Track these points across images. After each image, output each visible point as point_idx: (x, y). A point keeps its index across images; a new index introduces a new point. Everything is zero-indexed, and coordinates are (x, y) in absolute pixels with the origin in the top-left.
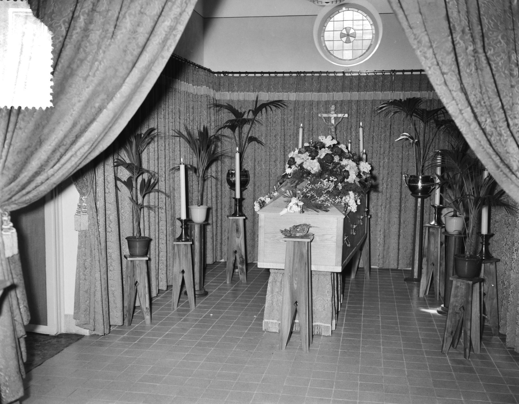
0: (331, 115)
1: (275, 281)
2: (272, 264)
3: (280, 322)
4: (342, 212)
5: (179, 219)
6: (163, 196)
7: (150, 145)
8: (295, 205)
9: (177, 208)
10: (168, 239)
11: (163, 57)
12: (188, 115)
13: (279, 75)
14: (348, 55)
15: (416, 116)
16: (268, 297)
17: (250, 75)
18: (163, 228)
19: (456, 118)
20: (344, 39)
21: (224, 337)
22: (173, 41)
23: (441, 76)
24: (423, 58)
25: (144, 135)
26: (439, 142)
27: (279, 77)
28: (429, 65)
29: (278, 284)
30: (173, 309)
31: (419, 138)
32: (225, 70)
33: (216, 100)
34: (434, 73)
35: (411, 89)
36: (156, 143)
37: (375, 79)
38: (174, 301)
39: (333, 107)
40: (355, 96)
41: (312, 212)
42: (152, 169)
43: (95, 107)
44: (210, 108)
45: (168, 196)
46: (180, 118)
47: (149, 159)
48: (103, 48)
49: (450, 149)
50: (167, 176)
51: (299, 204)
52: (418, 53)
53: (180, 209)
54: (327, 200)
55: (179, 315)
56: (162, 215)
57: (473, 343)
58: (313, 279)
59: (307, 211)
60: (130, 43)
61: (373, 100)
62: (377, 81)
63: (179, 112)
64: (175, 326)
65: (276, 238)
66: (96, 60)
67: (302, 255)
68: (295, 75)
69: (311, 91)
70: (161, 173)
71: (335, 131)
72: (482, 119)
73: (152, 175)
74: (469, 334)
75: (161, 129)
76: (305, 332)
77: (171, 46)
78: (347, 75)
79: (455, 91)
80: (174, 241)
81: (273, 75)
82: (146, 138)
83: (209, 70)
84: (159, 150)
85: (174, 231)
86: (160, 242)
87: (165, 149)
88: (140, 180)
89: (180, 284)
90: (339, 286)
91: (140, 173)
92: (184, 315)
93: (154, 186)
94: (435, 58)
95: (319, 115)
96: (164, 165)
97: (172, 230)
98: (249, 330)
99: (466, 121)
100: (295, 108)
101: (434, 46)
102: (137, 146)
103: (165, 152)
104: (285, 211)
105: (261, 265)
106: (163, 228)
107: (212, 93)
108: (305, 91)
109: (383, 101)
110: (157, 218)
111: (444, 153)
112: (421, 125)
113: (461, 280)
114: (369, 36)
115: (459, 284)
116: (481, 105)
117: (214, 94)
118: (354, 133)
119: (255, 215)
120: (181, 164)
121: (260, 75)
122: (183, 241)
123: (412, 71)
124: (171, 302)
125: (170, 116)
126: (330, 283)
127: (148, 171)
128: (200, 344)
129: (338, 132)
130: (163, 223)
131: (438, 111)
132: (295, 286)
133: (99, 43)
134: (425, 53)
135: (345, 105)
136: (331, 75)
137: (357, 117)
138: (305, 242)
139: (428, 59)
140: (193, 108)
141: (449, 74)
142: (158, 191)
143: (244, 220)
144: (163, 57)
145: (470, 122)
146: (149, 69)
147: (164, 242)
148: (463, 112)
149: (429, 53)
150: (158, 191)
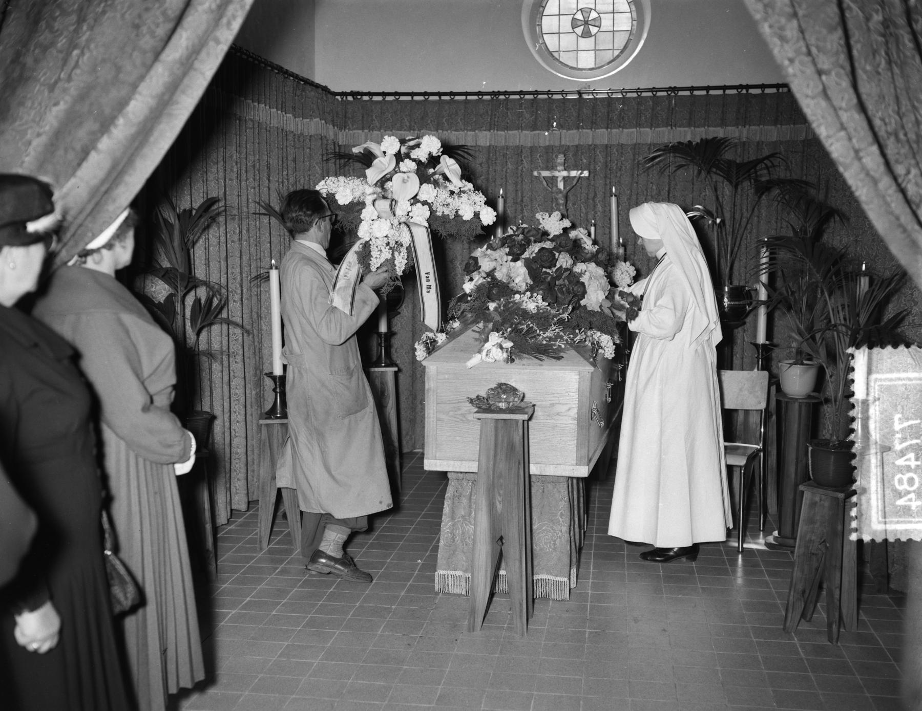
0: (556, 174)
1: (458, 496)
2: (452, 462)
3: (469, 575)
4: (587, 359)
5: (270, 375)
6: (238, 331)
7: (211, 231)
8: (496, 346)
9: (265, 352)
10: (249, 412)
11: (218, 42)
12: (285, 173)
13: (457, 98)
14: (586, 60)
15: (716, 173)
16: (446, 525)
17: (402, 98)
18: (238, 391)
19: (846, 167)
20: (579, 30)
21: (360, 606)
22: (238, 6)
23: (816, 77)
24: (776, 40)
25: (197, 211)
26: (759, 222)
27: (459, 102)
28: (791, 54)
29: (465, 501)
30: (261, 549)
31: (723, 213)
32: (356, 89)
33: (340, 146)
34: (803, 72)
35: (707, 123)
36: (222, 229)
37: (638, 104)
38: (263, 533)
39: (561, 159)
40: (602, 136)
41: (530, 361)
42: (214, 279)
43: (74, 149)
44: (328, 160)
45: (248, 332)
46: (269, 180)
47: (208, 260)
48: (90, 20)
49: (790, 234)
50: (245, 291)
51: (504, 346)
52: (766, 29)
53: (271, 355)
54: (558, 337)
55: (273, 561)
56: (237, 367)
57: (844, 611)
58: (533, 491)
59: (520, 358)
60: (147, 9)
61: (635, 144)
62: (642, 108)
63: (268, 168)
64: (262, 586)
65: (460, 412)
66: (75, 47)
67: (511, 447)
68: (488, 97)
69: (519, 128)
70: (234, 286)
71: (571, 202)
72: (900, 170)
73: (213, 291)
74: (837, 596)
75: (233, 200)
76: (520, 596)
77: (234, 17)
78: (585, 96)
79: (846, 111)
80: (261, 417)
81: (447, 98)
82: (201, 216)
83: (325, 89)
84: (229, 242)
85: (260, 398)
86: (232, 418)
87: (240, 240)
88: (190, 300)
89: (273, 499)
90: (582, 499)
91: (190, 285)
92: (282, 561)
93: (220, 312)
94: (804, 38)
95: (535, 173)
96: (238, 270)
97: (257, 394)
98: (408, 591)
99: (868, 174)
100: (489, 158)
101: (801, 13)
102: (183, 235)
103: (241, 244)
104: (476, 360)
105: (430, 465)
106: (238, 391)
107: (330, 132)
108: (507, 128)
109: (655, 145)
110: (226, 373)
111: (774, 246)
112: (727, 190)
113: (821, 491)
114: (625, 23)
115: (817, 499)
116: (898, 140)
117: (336, 135)
118: (600, 208)
119: (418, 372)
120: (271, 268)
121: (421, 98)
122: (277, 418)
123: (708, 88)
124: (256, 534)
125: (250, 175)
126: (566, 498)
127: (206, 284)
128: (312, 623)
129: (570, 204)
130: (237, 382)
131: (756, 166)
132: (499, 507)
133: (81, 9)
134: (782, 28)
135: (582, 153)
136: (555, 97)
137: (606, 177)
138: (517, 421)
139: (787, 42)
140: (295, 160)
141: (833, 73)
142: (229, 322)
143: (396, 373)
144: (218, 42)
145: (877, 175)
146: (188, 64)
147: (241, 418)
148: (861, 154)
149: (791, 30)
150: (229, 322)
